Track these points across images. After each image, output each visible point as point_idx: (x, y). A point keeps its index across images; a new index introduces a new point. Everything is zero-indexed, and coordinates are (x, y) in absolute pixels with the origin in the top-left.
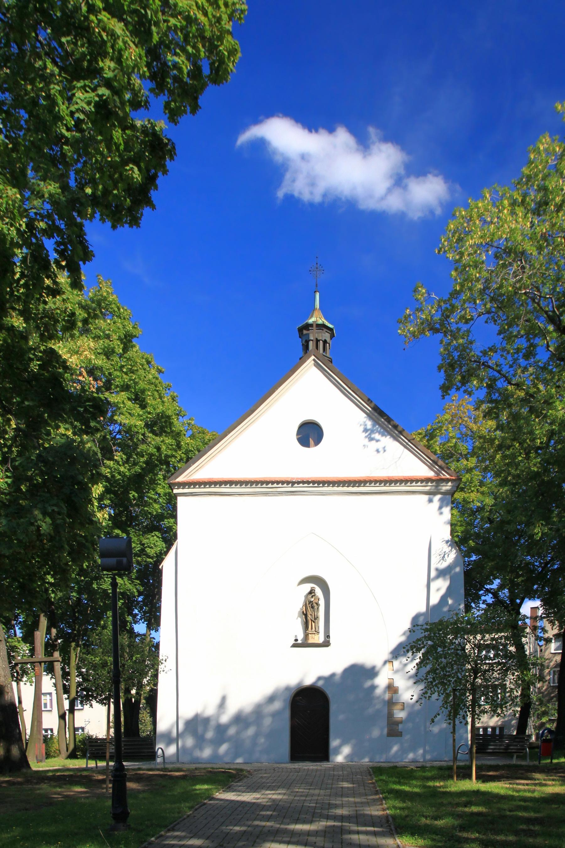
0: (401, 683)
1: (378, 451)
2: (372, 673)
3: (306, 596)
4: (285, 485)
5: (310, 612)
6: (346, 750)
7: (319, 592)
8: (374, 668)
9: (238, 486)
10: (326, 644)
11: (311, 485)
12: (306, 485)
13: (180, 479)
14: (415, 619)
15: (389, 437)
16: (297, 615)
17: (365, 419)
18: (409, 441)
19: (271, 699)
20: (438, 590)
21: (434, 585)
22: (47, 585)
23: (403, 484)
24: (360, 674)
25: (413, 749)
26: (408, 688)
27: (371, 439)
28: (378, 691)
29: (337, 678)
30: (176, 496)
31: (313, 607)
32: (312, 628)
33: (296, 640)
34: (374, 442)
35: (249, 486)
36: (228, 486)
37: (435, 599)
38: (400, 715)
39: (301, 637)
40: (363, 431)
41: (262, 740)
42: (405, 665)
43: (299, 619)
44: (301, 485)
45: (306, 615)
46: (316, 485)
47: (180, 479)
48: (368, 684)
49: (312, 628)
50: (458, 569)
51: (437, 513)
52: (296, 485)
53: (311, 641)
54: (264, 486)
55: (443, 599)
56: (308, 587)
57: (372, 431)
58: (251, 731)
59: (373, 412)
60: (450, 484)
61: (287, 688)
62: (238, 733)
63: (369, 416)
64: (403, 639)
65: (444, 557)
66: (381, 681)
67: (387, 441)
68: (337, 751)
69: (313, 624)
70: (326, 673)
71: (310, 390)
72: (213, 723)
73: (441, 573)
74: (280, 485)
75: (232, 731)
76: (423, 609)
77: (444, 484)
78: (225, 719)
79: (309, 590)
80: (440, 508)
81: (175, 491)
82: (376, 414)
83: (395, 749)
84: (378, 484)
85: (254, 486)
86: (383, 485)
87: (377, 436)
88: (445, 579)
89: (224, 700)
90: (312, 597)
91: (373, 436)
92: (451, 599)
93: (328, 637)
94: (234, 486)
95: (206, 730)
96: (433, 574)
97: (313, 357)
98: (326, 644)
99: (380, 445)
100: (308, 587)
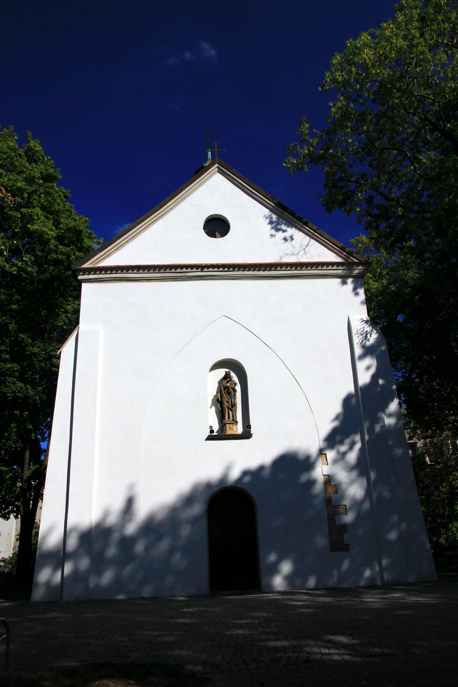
0: (342, 476)
1: (285, 239)
2: (307, 464)
3: (220, 382)
4: (194, 270)
5: (226, 399)
6: (286, 567)
7: (235, 378)
8: (308, 458)
9: (146, 271)
10: (246, 435)
11: (221, 269)
12: (216, 269)
13: (86, 266)
14: (347, 401)
15: (294, 228)
16: (210, 403)
17: (270, 213)
18: (314, 231)
19: (189, 500)
20: (368, 368)
21: (361, 365)
22: (413, 99)
23: (314, 268)
24: (292, 465)
25: (368, 564)
26: (352, 482)
27: (278, 230)
28: (319, 487)
29: (266, 473)
30: (80, 283)
31: (229, 393)
32: (229, 417)
33: (212, 431)
34: (281, 232)
35: (157, 271)
36: (135, 271)
37: (365, 378)
38: (349, 518)
39: (216, 428)
40: (269, 223)
41: (177, 558)
42: (344, 454)
43: (214, 408)
44: (211, 269)
45: (221, 403)
46: (226, 269)
47: (86, 266)
48: (304, 478)
49: (229, 417)
50: (383, 348)
51: (352, 294)
52: (206, 270)
53: (229, 432)
54: (173, 270)
55: (374, 378)
56: (221, 372)
57: (278, 223)
58: (164, 545)
59: (276, 207)
60: (360, 267)
61: (208, 486)
62: (148, 548)
63: (271, 210)
64: (336, 424)
65: (366, 336)
66: (320, 471)
67: (291, 231)
68: (274, 569)
69: (231, 413)
70: (253, 464)
71: (215, 192)
72: (116, 536)
73: (368, 351)
74: (189, 270)
75: (140, 547)
76: (351, 389)
77: (355, 267)
78: (131, 529)
79: (223, 374)
80: (355, 289)
81: (80, 277)
82: (280, 209)
83: (346, 565)
84: (289, 268)
85: (162, 271)
86: (294, 268)
87: (284, 227)
88: (373, 357)
89: (130, 503)
90: (228, 382)
91: (279, 227)
92: (382, 378)
93: (249, 426)
94: (141, 271)
95: (106, 546)
96: (358, 351)
97: (217, 165)
98: (246, 435)
99: (287, 235)
100: (221, 372)
